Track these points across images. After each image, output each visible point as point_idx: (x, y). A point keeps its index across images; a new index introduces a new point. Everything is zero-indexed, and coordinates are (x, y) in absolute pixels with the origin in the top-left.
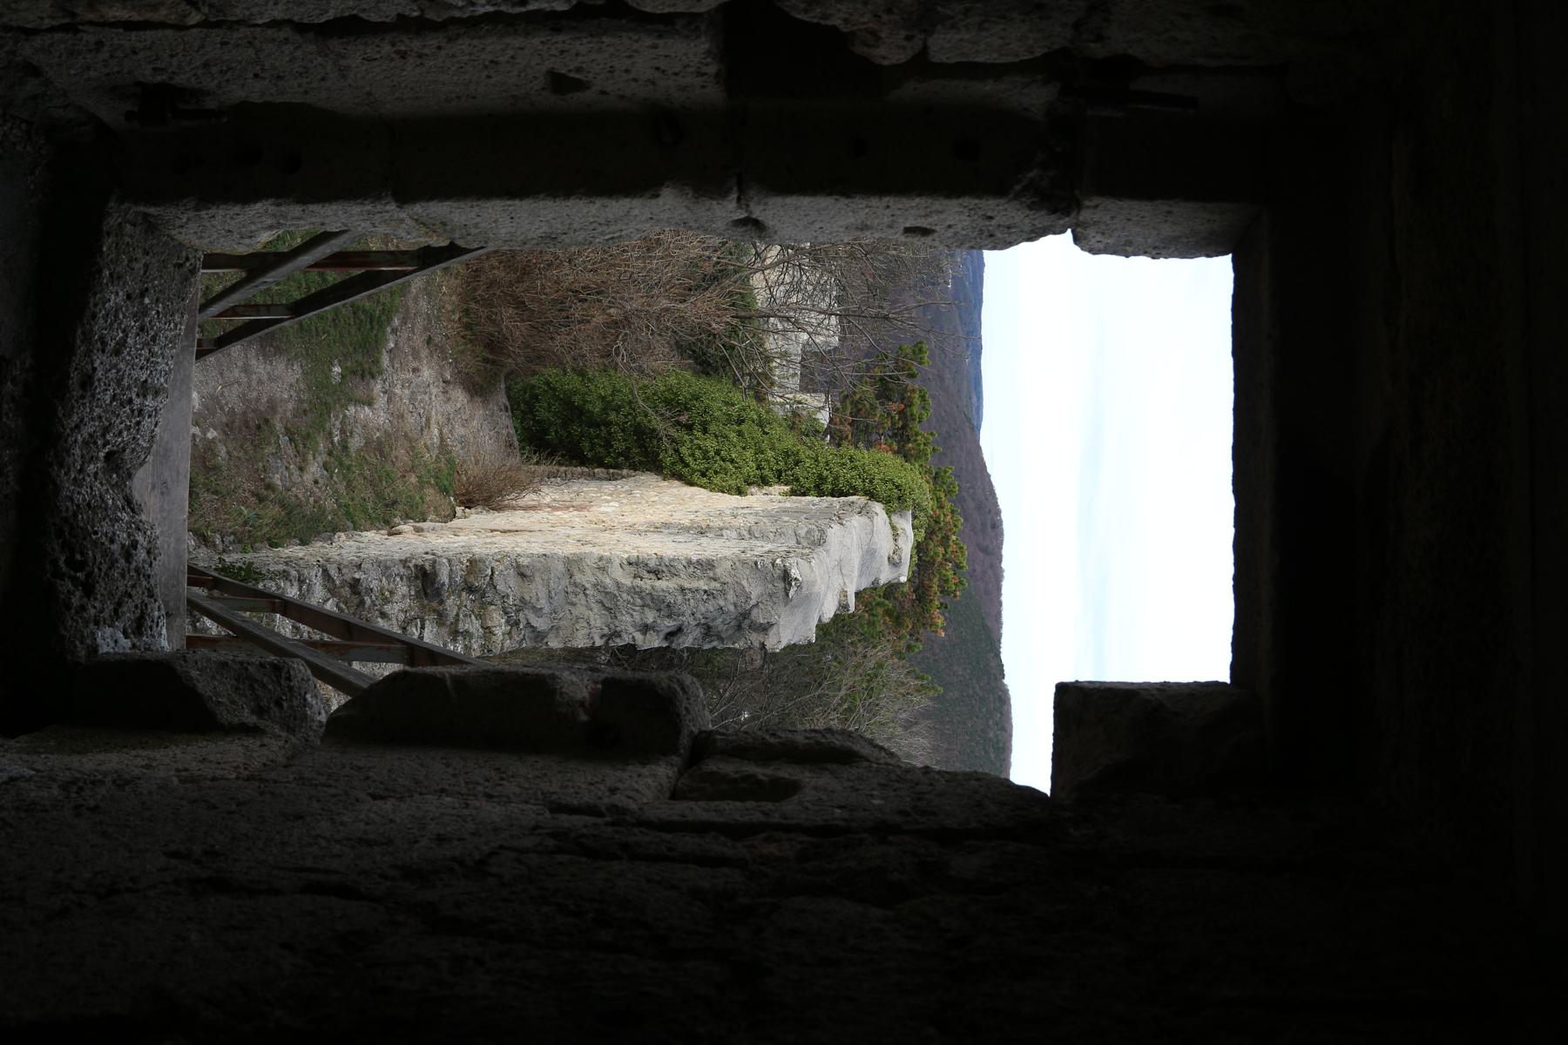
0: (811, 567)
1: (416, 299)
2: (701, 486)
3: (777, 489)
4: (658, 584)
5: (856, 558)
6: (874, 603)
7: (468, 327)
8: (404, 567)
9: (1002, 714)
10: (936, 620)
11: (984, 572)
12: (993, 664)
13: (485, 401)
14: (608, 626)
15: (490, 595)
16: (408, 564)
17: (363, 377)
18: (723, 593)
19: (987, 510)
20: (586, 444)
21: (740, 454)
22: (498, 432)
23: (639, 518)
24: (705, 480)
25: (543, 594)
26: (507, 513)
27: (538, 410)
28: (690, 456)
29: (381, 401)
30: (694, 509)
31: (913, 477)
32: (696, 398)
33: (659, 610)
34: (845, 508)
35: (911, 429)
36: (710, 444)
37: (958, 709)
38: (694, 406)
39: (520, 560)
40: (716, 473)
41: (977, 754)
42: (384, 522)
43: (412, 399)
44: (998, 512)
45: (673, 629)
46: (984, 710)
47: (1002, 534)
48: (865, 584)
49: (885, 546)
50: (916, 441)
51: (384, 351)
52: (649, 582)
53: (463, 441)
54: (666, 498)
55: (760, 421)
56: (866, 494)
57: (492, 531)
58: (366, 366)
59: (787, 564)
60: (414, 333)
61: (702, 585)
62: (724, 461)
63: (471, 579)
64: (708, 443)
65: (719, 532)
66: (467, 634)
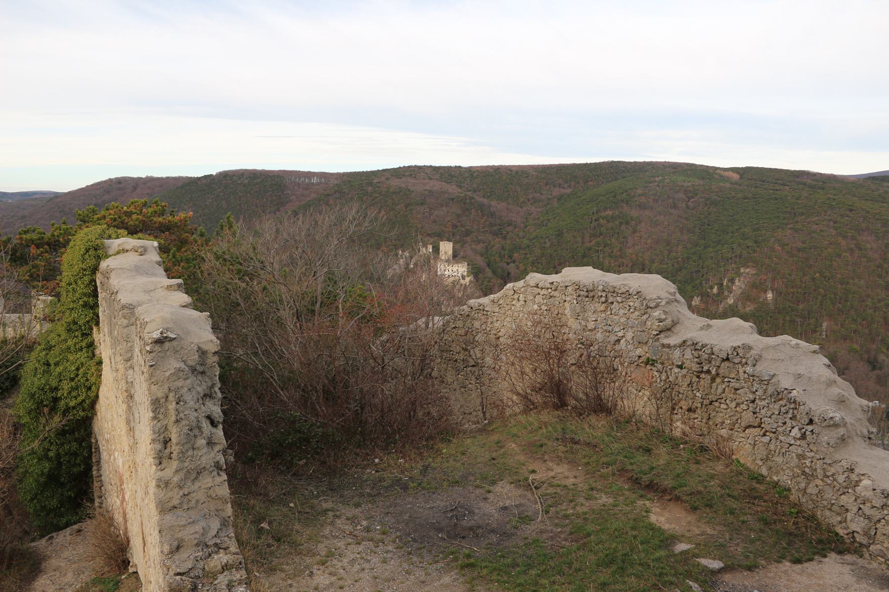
0: (151, 321)
2: (98, 390)
3: (96, 335)
4: (174, 440)
5: (143, 280)
6: (174, 260)
9: (234, 175)
10: (182, 218)
11: (149, 188)
12: (204, 181)
13: (45, 558)
14: (211, 472)
15: (195, 573)
18: (178, 389)
19: (109, 187)
20: (75, 470)
21: (72, 364)
22: (70, 544)
23: (125, 442)
24: (93, 388)
25: (191, 529)
26: (130, 534)
28: (76, 399)
30: (114, 399)
31: (82, 237)
32: (32, 396)
33: (195, 436)
34: (106, 289)
35: (49, 240)
36: (66, 386)
38: (39, 397)
39: (166, 551)
40: (87, 380)
41: (258, 190)
44: (110, 180)
45: (208, 422)
46: (232, 186)
48: (161, 271)
49: (131, 259)
50: (58, 236)
52: (173, 448)
53: (78, 573)
54: (109, 416)
57: (144, 552)
59: (150, 341)
61: (172, 406)
62: (77, 375)
64: (66, 387)
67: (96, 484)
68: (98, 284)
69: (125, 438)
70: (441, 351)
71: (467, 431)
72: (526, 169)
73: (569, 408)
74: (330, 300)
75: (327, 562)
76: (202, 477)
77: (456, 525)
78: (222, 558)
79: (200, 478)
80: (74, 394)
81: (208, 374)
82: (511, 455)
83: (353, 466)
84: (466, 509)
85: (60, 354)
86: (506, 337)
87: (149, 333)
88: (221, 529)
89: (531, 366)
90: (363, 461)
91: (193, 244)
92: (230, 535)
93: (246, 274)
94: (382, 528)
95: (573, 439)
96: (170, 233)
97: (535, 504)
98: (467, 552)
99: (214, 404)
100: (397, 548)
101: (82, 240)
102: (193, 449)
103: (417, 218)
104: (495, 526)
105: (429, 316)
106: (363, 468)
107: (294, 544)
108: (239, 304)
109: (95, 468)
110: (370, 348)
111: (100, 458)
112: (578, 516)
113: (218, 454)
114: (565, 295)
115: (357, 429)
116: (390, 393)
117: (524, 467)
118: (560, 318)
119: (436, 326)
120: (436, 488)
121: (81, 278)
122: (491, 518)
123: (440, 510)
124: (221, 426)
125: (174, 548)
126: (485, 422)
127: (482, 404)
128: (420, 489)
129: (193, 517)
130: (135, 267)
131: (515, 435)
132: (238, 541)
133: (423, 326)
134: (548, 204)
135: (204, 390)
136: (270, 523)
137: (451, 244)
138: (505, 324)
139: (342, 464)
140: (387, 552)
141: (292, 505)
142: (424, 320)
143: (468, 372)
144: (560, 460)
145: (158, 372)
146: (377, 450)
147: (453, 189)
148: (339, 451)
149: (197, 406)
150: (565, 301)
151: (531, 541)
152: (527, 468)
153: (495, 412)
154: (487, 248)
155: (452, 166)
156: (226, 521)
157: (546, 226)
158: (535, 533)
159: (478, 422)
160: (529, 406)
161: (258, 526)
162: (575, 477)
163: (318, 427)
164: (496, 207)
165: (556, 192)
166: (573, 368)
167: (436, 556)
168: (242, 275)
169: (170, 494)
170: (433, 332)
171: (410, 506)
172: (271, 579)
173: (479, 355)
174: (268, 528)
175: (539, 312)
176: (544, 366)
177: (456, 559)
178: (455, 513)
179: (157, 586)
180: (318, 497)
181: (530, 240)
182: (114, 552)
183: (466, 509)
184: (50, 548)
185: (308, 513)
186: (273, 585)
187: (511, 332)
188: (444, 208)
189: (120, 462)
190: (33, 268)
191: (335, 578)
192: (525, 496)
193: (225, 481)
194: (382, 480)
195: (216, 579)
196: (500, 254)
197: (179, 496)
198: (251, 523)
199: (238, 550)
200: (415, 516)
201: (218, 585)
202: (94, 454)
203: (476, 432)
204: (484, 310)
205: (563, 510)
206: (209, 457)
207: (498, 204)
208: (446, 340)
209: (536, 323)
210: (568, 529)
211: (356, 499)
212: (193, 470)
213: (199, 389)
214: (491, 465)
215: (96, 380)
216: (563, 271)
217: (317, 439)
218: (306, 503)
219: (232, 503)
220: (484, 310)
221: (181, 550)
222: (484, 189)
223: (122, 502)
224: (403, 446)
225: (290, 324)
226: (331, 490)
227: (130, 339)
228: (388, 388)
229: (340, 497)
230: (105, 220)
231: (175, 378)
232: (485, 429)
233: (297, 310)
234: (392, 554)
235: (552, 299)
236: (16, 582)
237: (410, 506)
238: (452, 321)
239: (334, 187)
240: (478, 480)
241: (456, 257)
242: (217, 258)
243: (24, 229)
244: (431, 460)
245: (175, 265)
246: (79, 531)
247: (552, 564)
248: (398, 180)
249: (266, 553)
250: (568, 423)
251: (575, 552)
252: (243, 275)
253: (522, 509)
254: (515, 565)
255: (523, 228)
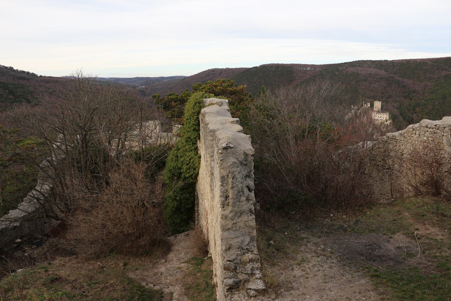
0: (222, 139)
1: (137, 275)
2: (199, 170)
4: (230, 197)
5: (220, 118)
6: (236, 109)
7: (147, 255)
8: (228, 297)
9: (268, 67)
10: (241, 88)
16: (226, 295)
17: (163, 297)
18: (233, 172)
21: (188, 157)
22: (183, 240)
23: (209, 196)
24: (197, 169)
25: (236, 240)
26: (209, 239)
27: (178, 222)
28: (189, 174)
29: (171, 289)
30: (205, 175)
32: (170, 171)
33: (241, 196)
34: (203, 122)
35: (180, 98)
36: (185, 167)
37: (267, 80)
39: (224, 249)
40: (194, 165)
41: (280, 73)
42: (213, 288)
43: (171, 275)
44: (209, 70)
46: (267, 72)
47: (215, 69)
48: (229, 114)
49: (215, 108)
50: (184, 97)
51: (154, 288)
52: (230, 200)
53: (186, 254)
55: (177, 150)
56: (199, 115)
58: (159, 296)
60: (148, 276)
61: (230, 180)
62: (190, 163)
63: (231, 269)
65: (212, 168)
66: (252, 269)
67: (196, 214)
68: (200, 120)
69: (209, 194)
70: (370, 160)
71: (382, 203)
72: (425, 61)
73: (442, 196)
74: (312, 131)
75: (301, 264)
76: (243, 215)
77: (371, 253)
78: (249, 256)
79: (242, 216)
80: (188, 171)
81: (248, 165)
82: (405, 219)
83: (319, 217)
84: (377, 246)
85: (183, 152)
86: (407, 154)
87: (221, 144)
88: (250, 242)
89: (421, 171)
90: (324, 215)
91: (246, 101)
92: (254, 245)
93: (271, 116)
94: (331, 250)
95: (443, 214)
96: (235, 95)
97: (417, 247)
98: (376, 268)
99: (251, 180)
100: (338, 262)
101: (193, 99)
102: (239, 202)
103: (362, 88)
104: (392, 256)
105: (364, 141)
106: (324, 218)
107: (286, 253)
108: (267, 131)
109: (196, 206)
110: (332, 156)
111: (198, 202)
112: (443, 257)
113: (251, 205)
114: (444, 132)
115: (323, 198)
116: (341, 180)
117: (412, 227)
118: (440, 145)
119: (368, 147)
120: (362, 233)
121: (192, 117)
122: (391, 252)
123: (363, 245)
124: (253, 192)
125: (227, 248)
126: (392, 199)
127: (391, 189)
128: (353, 232)
129: (237, 235)
130: (217, 112)
131: (409, 208)
132: (258, 248)
133: (361, 146)
134: (438, 80)
135: (246, 173)
136: (274, 241)
137: (381, 102)
138: (407, 147)
139: (313, 216)
140: (332, 263)
141: (286, 233)
142: (361, 143)
143: (385, 172)
144: (434, 225)
145: (224, 163)
146: (332, 209)
147: (382, 73)
148: (313, 208)
149: (242, 181)
150: (443, 136)
151: (413, 268)
152: (414, 227)
153: (398, 195)
154: (400, 105)
155: (382, 60)
156: (253, 238)
157: (436, 93)
158: (415, 263)
159: (389, 200)
160: (418, 193)
161: (268, 242)
162: (443, 235)
163: (303, 196)
164: (407, 82)
165: (444, 73)
166: (446, 174)
167: (358, 268)
168: (269, 116)
169: (227, 222)
170: (366, 150)
171: (347, 240)
172: (272, 269)
173: (391, 163)
174: (273, 243)
175: (428, 141)
176: (428, 171)
177: (369, 272)
178: (371, 247)
179: (219, 265)
180: (300, 231)
181: (426, 100)
182: (202, 246)
183: (377, 246)
184: (175, 241)
185: (294, 238)
186: (273, 272)
187: (410, 152)
188: (377, 83)
189: (207, 205)
190: (173, 112)
191: (304, 273)
192: (411, 242)
193: (253, 218)
194: (333, 225)
195: (246, 266)
196: (408, 109)
197: (231, 224)
198: (265, 240)
199: (257, 253)
200: (349, 246)
201: (247, 269)
202: (196, 200)
203: (387, 205)
204: (395, 139)
205: (434, 253)
206: (247, 206)
207: (408, 80)
208: (373, 154)
209: (425, 148)
210: (435, 264)
211: (319, 234)
212: (239, 212)
213: (243, 172)
214: (393, 223)
215: (198, 165)
216: (443, 118)
217: (301, 202)
218: (293, 233)
219: (257, 230)
220: (395, 139)
221: (231, 249)
222: (400, 72)
223: (207, 224)
224: (346, 209)
225: (292, 142)
226: (307, 228)
227: (213, 147)
228: (341, 178)
229: (311, 232)
230: (205, 89)
231: (232, 166)
232: (392, 204)
233: (296, 135)
234: (335, 264)
235: (435, 134)
236: (161, 254)
237: (347, 240)
238: (377, 144)
239: (319, 72)
240: (385, 231)
241: (383, 110)
242: (257, 108)
243: (170, 94)
244: (360, 217)
245: (237, 111)
246: (188, 235)
247: (424, 282)
248: (352, 68)
249: (271, 256)
250: (441, 205)
251: (439, 278)
252: (269, 117)
253: (409, 249)
254: (402, 279)
255: (422, 94)
